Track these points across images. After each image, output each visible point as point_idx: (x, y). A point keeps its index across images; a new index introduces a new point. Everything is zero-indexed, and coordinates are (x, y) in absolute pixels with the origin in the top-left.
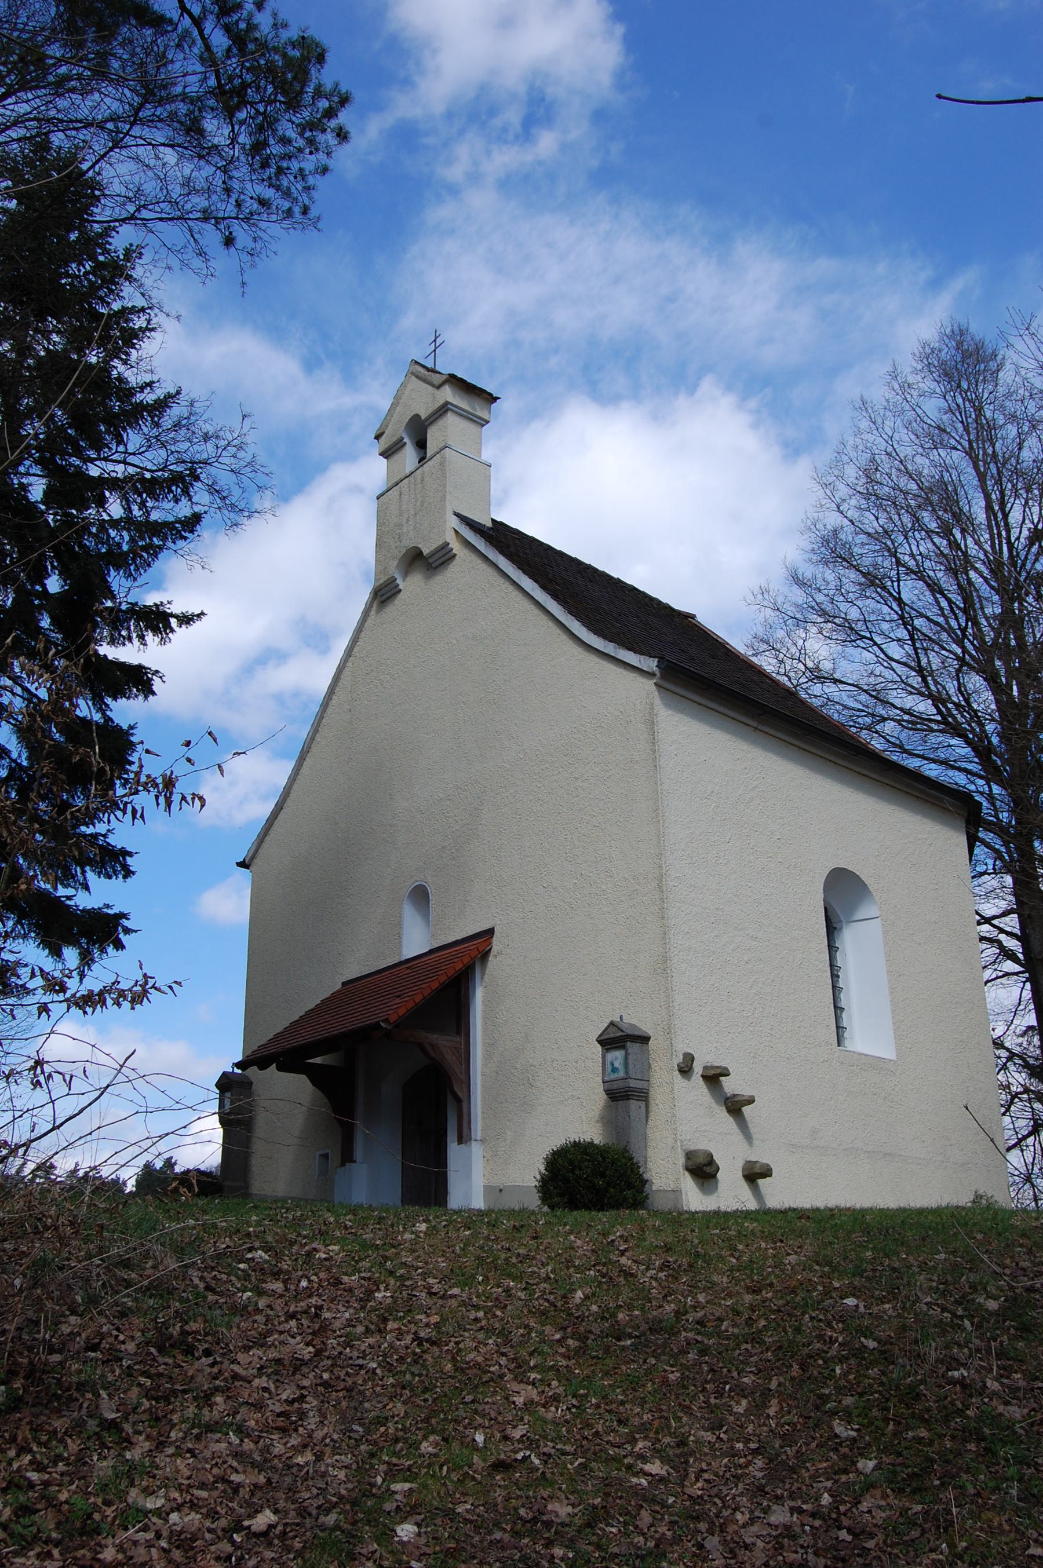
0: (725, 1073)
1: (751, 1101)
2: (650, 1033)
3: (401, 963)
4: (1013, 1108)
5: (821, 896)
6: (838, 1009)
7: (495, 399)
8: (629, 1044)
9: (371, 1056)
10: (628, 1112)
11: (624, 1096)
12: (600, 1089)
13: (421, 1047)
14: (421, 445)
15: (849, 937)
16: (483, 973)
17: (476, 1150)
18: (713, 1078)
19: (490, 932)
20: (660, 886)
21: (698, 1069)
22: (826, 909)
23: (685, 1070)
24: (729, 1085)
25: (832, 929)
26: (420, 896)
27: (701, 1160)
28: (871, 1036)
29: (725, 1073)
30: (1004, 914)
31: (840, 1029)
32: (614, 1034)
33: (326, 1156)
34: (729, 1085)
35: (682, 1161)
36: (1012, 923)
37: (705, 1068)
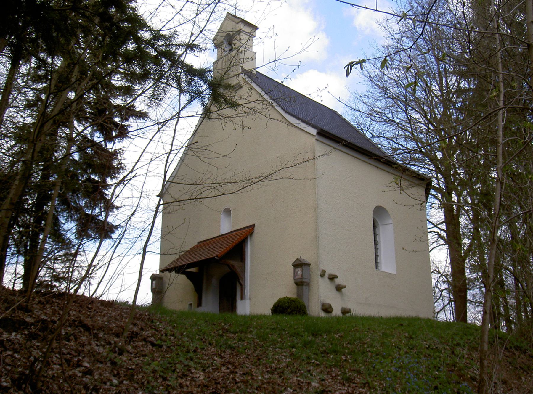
0: (336, 277)
1: (345, 287)
2: (311, 262)
3: (220, 236)
4: (485, 363)
5: (372, 216)
6: (376, 256)
7: (258, 28)
8: (303, 267)
9: (211, 268)
10: (302, 289)
11: (301, 284)
12: (293, 281)
13: (228, 266)
14: (230, 44)
15: (381, 230)
16: (251, 240)
17: (247, 302)
18: (332, 278)
19: (253, 226)
20: (315, 211)
21: (327, 275)
22: (374, 221)
23: (322, 276)
24: (338, 281)
25: (375, 227)
26: (228, 211)
27: (327, 306)
28: (388, 265)
29: (336, 277)
30: (441, 223)
31: (377, 263)
32: (298, 263)
33: (191, 305)
34: (338, 281)
35: (320, 307)
36: (444, 227)
37: (329, 275)
